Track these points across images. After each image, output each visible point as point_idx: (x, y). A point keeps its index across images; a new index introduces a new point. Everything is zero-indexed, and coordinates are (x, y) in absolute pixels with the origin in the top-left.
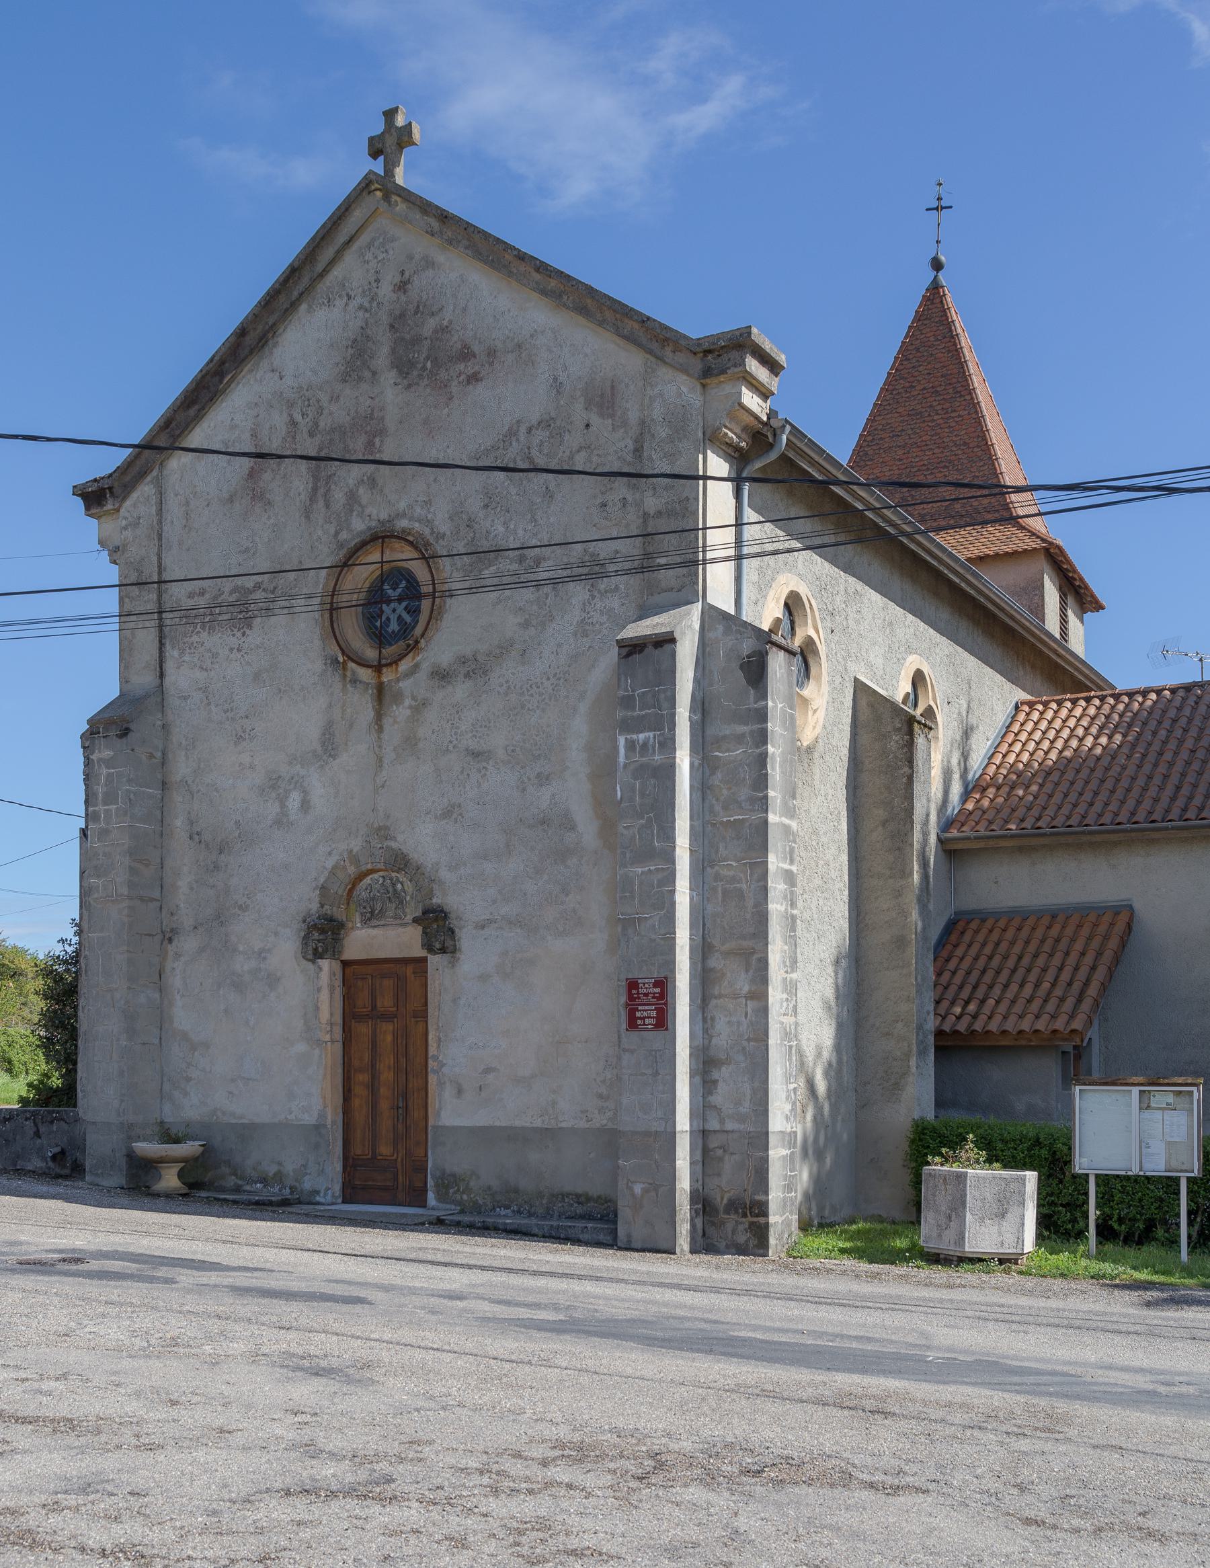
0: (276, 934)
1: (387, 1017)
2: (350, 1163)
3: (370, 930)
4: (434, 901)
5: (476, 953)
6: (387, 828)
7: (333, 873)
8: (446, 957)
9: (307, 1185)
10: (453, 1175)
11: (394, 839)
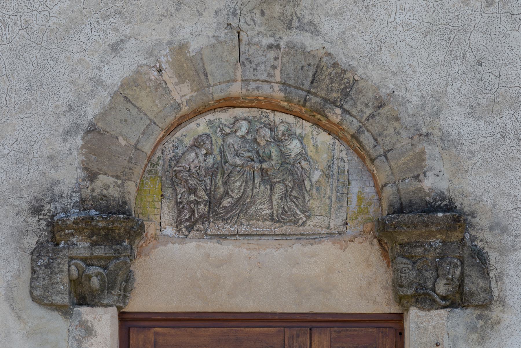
4: (428, 183)
7: (125, 95)
8: (461, 318)
11: (313, 28)
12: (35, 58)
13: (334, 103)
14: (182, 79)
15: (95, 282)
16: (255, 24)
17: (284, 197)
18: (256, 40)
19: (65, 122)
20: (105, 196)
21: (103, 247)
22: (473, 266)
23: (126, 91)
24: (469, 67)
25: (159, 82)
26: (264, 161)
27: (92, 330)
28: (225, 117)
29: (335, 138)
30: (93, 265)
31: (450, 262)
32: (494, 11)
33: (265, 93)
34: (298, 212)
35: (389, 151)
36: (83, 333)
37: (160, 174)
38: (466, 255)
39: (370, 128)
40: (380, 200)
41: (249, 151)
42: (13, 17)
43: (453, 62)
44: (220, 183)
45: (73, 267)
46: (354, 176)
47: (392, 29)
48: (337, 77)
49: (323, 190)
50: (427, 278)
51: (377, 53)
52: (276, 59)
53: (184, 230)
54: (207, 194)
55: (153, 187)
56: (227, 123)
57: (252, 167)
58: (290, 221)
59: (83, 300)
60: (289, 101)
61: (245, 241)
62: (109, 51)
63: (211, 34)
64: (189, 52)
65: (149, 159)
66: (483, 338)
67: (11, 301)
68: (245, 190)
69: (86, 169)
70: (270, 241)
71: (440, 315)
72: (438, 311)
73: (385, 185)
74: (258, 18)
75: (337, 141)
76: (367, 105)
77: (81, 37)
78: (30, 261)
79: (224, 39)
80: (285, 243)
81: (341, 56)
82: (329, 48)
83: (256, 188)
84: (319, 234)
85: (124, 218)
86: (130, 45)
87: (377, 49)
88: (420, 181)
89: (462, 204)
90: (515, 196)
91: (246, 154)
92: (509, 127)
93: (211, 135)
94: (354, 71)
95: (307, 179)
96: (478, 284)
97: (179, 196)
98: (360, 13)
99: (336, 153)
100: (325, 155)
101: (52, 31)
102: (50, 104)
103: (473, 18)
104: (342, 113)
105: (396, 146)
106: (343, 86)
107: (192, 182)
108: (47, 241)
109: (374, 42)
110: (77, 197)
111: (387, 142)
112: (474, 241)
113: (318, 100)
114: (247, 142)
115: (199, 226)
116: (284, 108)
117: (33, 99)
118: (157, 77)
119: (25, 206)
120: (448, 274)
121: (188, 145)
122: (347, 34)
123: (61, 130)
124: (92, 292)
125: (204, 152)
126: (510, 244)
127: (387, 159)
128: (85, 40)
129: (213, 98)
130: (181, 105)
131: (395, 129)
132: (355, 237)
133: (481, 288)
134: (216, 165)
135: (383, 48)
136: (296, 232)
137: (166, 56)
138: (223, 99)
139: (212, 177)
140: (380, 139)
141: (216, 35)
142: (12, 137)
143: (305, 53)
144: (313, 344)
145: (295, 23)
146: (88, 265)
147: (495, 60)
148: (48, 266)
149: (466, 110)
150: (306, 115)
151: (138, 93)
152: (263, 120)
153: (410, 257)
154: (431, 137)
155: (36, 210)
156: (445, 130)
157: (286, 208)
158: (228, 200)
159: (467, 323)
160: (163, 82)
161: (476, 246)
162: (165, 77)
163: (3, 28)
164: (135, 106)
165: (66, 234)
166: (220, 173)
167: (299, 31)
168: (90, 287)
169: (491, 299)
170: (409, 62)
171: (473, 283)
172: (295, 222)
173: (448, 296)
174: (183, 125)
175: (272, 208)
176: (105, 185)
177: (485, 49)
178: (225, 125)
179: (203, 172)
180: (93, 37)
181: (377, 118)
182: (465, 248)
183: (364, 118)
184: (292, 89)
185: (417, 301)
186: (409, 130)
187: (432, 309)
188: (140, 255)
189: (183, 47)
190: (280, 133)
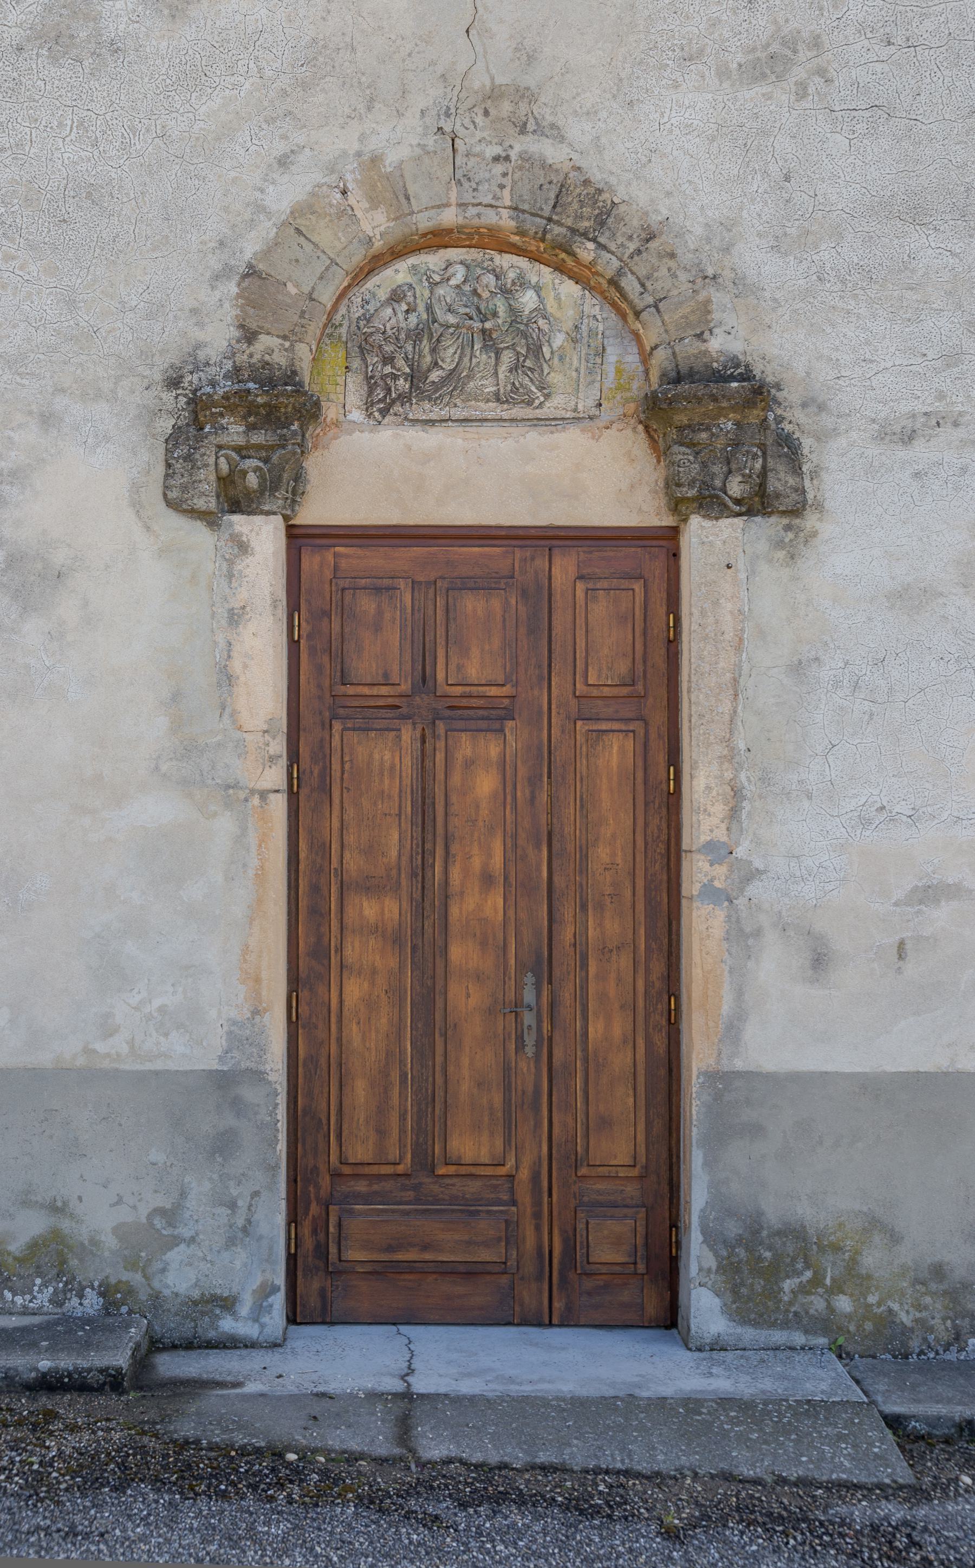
0: (47, 420)
1: (493, 716)
2: (315, 1190)
3: (413, 435)
4: (716, 344)
5: (869, 517)
6: (525, 94)
7: (296, 226)
8: (763, 529)
9: (180, 1277)
10: (795, 1233)
11: (556, 133)
12: (174, 176)
13: (585, 235)
14: (374, 203)
15: (252, 480)
16: (475, 127)
17: (513, 369)
18: (477, 149)
19: (215, 263)
20: (268, 364)
21: (263, 432)
22: (779, 456)
23: (298, 221)
24: (772, 184)
25: (342, 208)
26: (487, 320)
27: (248, 546)
28: (433, 261)
29: (584, 288)
30: (249, 458)
31: (748, 452)
32: (808, 106)
33: (488, 222)
34: (533, 389)
35: (661, 300)
36: (236, 550)
37: (344, 339)
38: (769, 442)
39: (635, 269)
40: (647, 372)
41: (466, 306)
42: (146, 121)
43: (750, 177)
44: (427, 350)
45: (222, 460)
46: (611, 339)
47: (665, 133)
48: (589, 199)
49: (567, 359)
50: (714, 474)
51: (644, 166)
52: (505, 175)
53: (376, 414)
54: (408, 366)
55: (335, 356)
56: (436, 269)
57: (470, 328)
58: (523, 401)
59: (236, 507)
60: (521, 233)
61: (461, 429)
62: (276, 166)
63: (415, 142)
64: (385, 167)
65: (330, 319)
66: (792, 557)
67: (137, 506)
68: (460, 358)
69: (242, 326)
70: (494, 429)
71: (732, 525)
72: (730, 520)
73: (656, 347)
74: (479, 120)
75: (587, 292)
76: (630, 238)
77: (237, 148)
78: (164, 452)
79: (433, 149)
80: (515, 430)
81: (595, 170)
82: (579, 161)
83: (476, 357)
84: (563, 419)
85: (292, 391)
86: (303, 158)
87: (644, 159)
88: (705, 341)
89: (763, 372)
90: (838, 360)
91: (463, 310)
92: (828, 265)
93: (414, 285)
94: (613, 191)
95: (546, 344)
96: (786, 482)
97: (370, 368)
98: (620, 111)
99: (586, 308)
100: (571, 312)
101: (197, 139)
102: (193, 239)
103: (777, 117)
104: (596, 248)
105: (671, 294)
106: (597, 212)
107: (388, 348)
108: (187, 425)
109: (641, 150)
110: (228, 365)
111: (659, 288)
112: (780, 422)
113: (563, 230)
114: (464, 295)
115: (397, 408)
116: (514, 245)
117: (171, 231)
118: (341, 201)
119: (158, 377)
120: (745, 467)
121: (383, 299)
122: (603, 140)
123: (208, 274)
124: (248, 493)
125: (405, 307)
126: (831, 426)
127: (658, 311)
128: (242, 152)
129: (417, 230)
130: (374, 240)
131: (669, 269)
132: (612, 423)
133: (791, 487)
134: (421, 326)
135: (653, 159)
136: (530, 416)
137: (353, 172)
138: (431, 233)
139: (415, 342)
140: (648, 284)
141: (422, 143)
142: (142, 283)
143: (546, 167)
144: (553, 569)
145: (531, 126)
146: (243, 457)
147: (809, 173)
148: (188, 458)
149: (768, 242)
150: (545, 255)
151: (314, 222)
152: (486, 265)
153: (691, 445)
154: (720, 280)
155: (174, 383)
156: (739, 271)
157: (517, 384)
158: (438, 373)
159: (770, 536)
160: (348, 208)
161: (783, 429)
162: (352, 200)
163: (131, 136)
164: (310, 241)
165: (212, 414)
166: (426, 337)
167: (536, 137)
168: (245, 487)
169: (805, 502)
170: (689, 178)
171: (779, 480)
172: (529, 403)
173: (743, 499)
174: (376, 272)
175: (498, 385)
176: (269, 348)
177: (795, 159)
178: (434, 272)
179: (403, 336)
180: (254, 148)
181: (644, 254)
182: (768, 432)
183: (627, 255)
184: (526, 215)
185: (701, 506)
186: (690, 271)
187: (721, 518)
188: (315, 447)
189: (376, 160)
190: (509, 281)
